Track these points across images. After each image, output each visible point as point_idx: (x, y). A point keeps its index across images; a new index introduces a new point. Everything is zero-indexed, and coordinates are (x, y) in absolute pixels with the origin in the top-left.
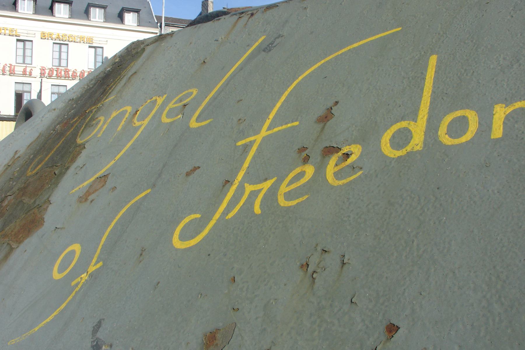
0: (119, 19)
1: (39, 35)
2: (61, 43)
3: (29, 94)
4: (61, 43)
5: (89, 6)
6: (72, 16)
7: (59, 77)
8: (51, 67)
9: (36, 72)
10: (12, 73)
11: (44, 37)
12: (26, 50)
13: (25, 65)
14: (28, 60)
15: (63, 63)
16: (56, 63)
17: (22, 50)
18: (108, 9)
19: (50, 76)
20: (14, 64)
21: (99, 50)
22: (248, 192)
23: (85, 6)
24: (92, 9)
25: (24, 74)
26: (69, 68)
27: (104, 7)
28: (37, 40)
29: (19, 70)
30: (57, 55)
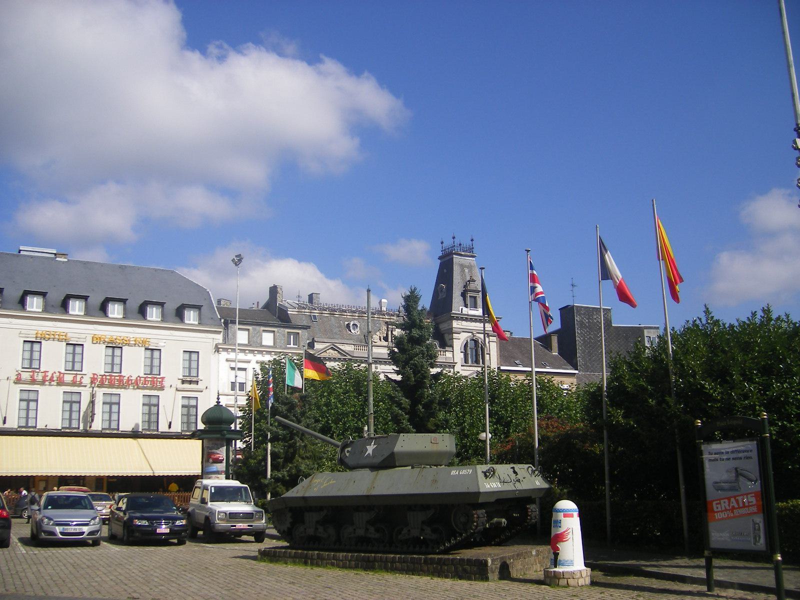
0: (101, 312)
1: (89, 339)
2: (114, 346)
3: (78, 405)
4: (114, 346)
5: (26, 293)
6: (164, 320)
7: (111, 386)
8: (103, 373)
9: (86, 380)
10: (61, 383)
11: (96, 340)
12: (192, 362)
13: (75, 372)
14: (77, 366)
15: (117, 369)
16: (109, 369)
17: (150, 360)
18: (89, 300)
19: (101, 385)
20: (63, 371)
21: (194, 356)
22: (325, 485)
23: (21, 293)
24: (29, 299)
25: (74, 383)
26: (123, 374)
27: (43, 294)
28: (88, 345)
29: (68, 378)
30: (27, 355)
